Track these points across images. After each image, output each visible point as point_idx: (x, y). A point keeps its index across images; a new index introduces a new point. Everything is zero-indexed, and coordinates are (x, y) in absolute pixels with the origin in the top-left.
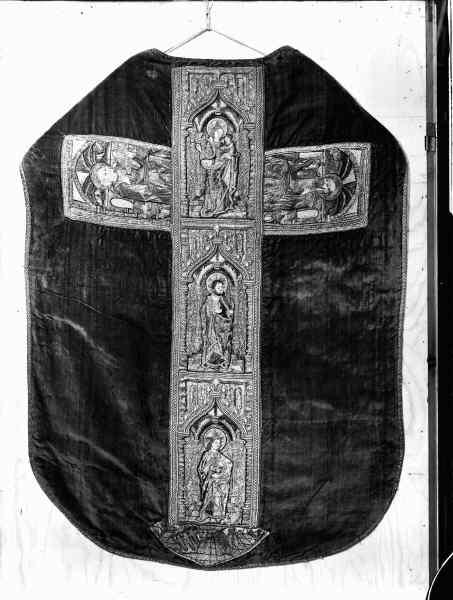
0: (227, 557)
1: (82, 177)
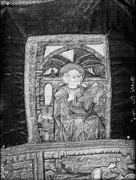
1: (69, 55)
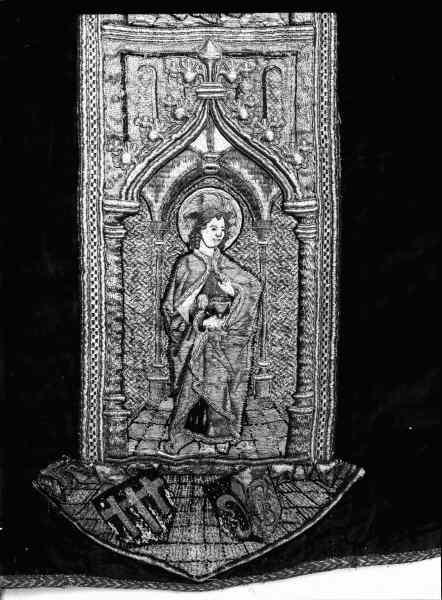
0: (251, 547)
